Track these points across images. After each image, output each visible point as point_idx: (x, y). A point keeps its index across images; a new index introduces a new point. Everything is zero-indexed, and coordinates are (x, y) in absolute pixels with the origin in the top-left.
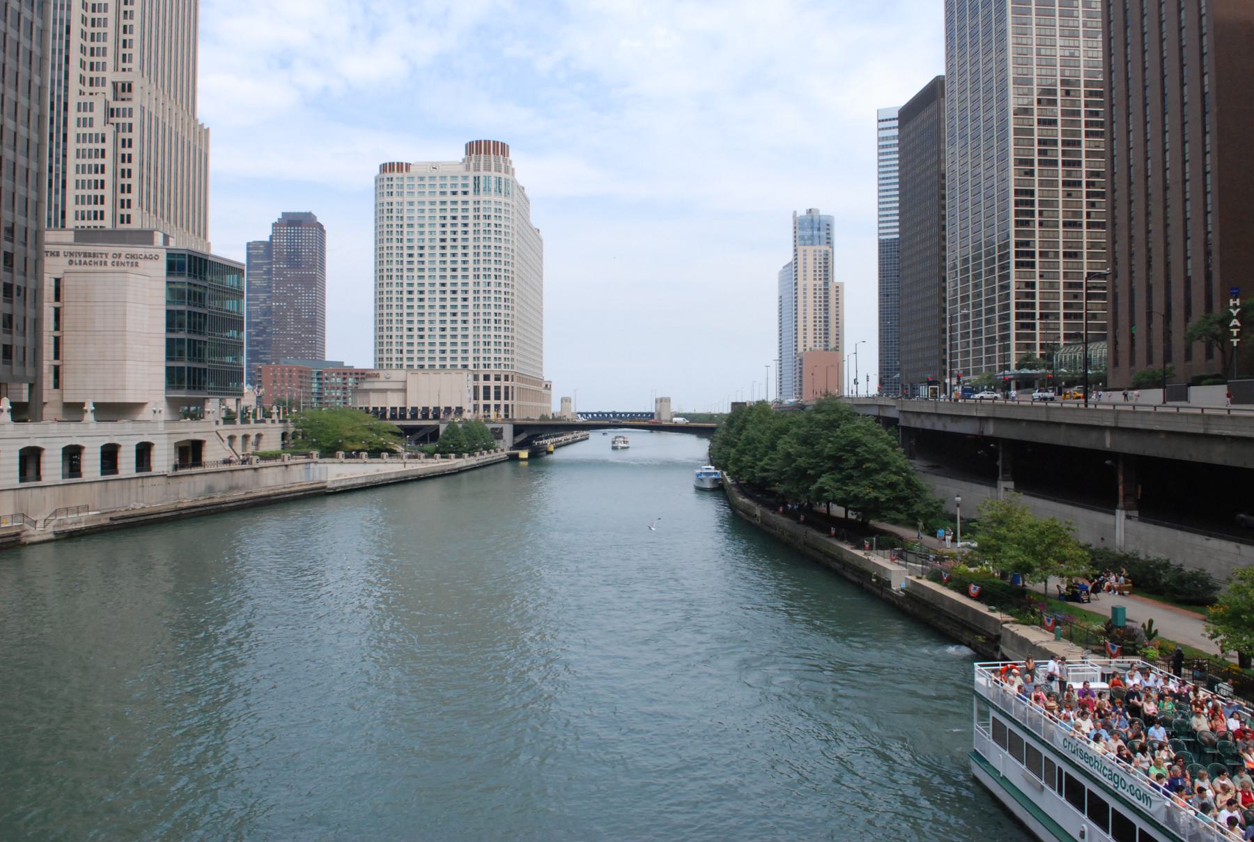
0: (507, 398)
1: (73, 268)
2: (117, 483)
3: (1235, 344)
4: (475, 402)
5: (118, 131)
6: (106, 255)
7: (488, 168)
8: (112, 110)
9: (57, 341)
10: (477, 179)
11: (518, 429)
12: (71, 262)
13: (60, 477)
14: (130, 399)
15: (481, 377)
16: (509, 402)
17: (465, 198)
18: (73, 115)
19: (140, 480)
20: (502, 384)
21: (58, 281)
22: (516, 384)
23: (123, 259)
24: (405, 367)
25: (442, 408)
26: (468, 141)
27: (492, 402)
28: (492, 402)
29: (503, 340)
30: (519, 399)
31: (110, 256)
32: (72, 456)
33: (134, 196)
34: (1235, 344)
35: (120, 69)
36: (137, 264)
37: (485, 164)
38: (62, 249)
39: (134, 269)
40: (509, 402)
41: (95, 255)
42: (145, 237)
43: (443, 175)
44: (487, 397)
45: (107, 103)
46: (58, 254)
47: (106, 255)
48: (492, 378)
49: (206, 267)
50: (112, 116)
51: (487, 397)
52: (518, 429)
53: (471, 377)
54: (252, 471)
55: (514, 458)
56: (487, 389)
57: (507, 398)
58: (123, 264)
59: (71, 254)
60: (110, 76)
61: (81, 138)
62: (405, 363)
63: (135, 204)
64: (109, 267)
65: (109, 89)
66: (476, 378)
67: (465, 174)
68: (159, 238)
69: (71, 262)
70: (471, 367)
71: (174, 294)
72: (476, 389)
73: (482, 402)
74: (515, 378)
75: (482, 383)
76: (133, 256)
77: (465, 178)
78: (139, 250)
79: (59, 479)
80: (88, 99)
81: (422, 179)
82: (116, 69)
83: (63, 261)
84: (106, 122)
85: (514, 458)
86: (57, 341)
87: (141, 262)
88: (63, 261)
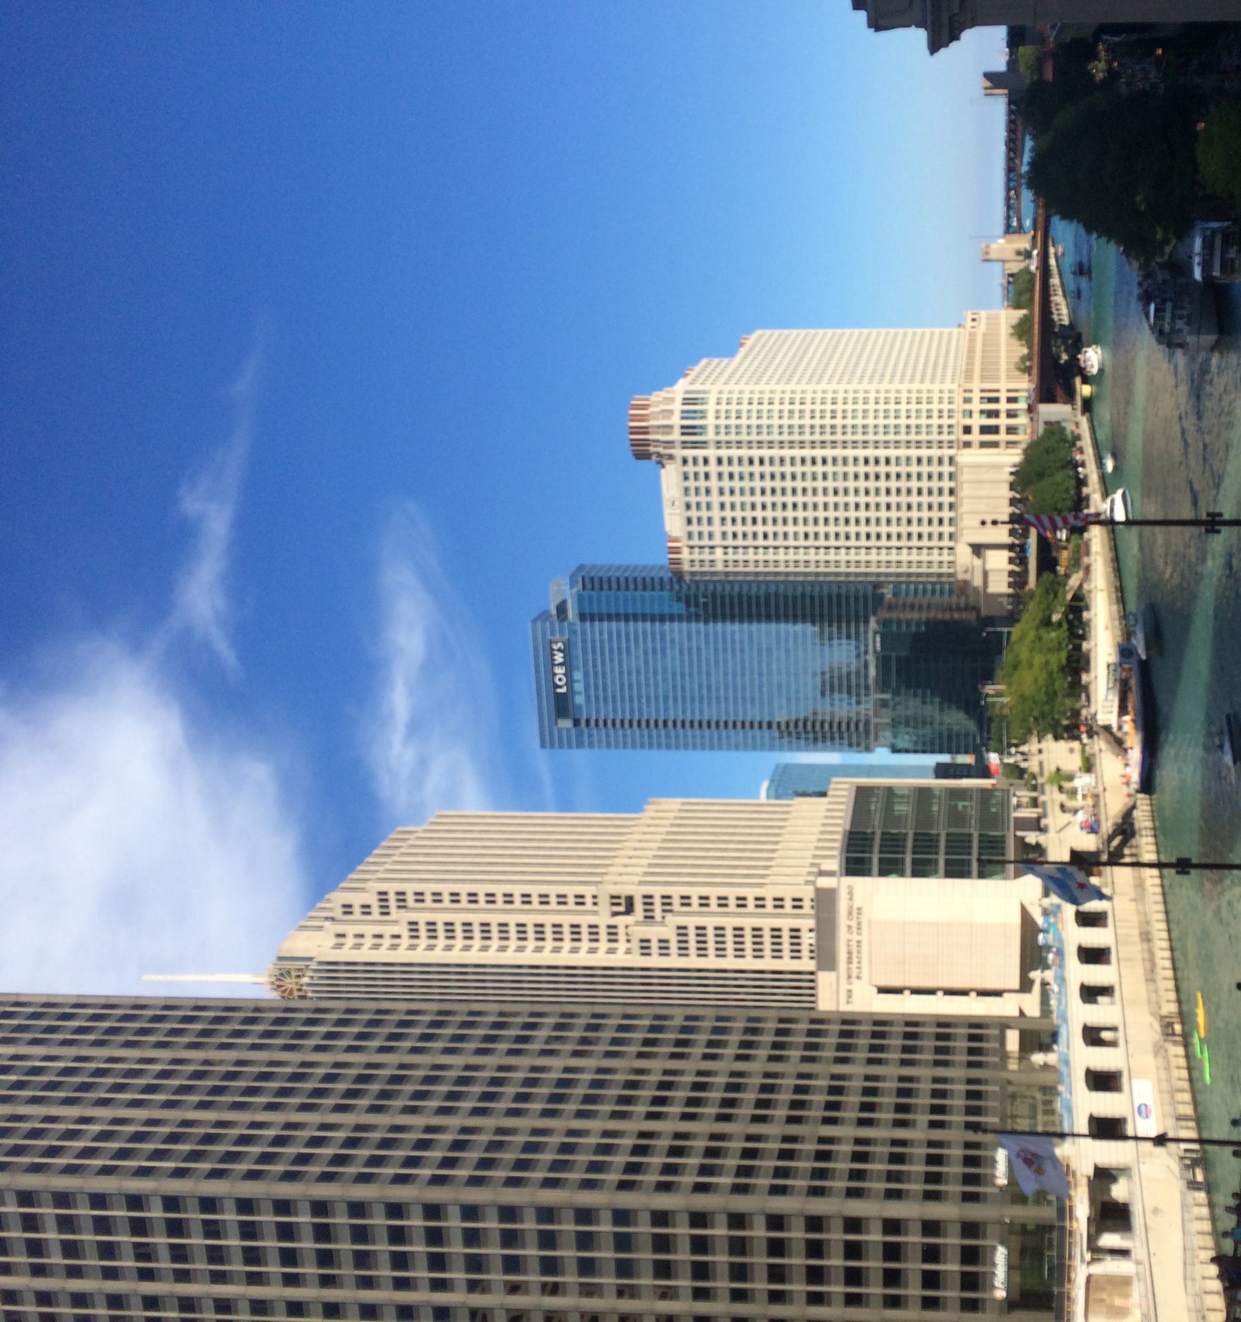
0: (996, 400)
1: (865, 974)
2: (1120, 948)
3: (1062, 362)
4: (1003, 445)
5: (670, 911)
6: (849, 941)
7: (668, 428)
8: (646, 917)
9: (950, 992)
10: (685, 445)
11: (1046, 394)
12: (859, 978)
13: (1114, 1008)
14: (1016, 919)
15: (967, 438)
16: (1003, 396)
17: (713, 461)
18: (655, 961)
19: (1117, 924)
20: (976, 406)
21: (883, 990)
22: (976, 385)
23: (854, 923)
24: (951, 544)
25: (1012, 494)
26: (633, 458)
27: (1003, 421)
28: (1003, 421)
29: (913, 407)
30: (996, 379)
31: (850, 937)
32: (1091, 993)
33: (750, 893)
34: (1062, 362)
35: (595, 908)
36: (859, 909)
37: (664, 433)
38: (844, 986)
39: (864, 911)
40: (1003, 396)
41: (850, 953)
42: (825, 902)
43: (682, 491)
44: (994, 430)
45: (637, 923)
46: (849, 991)
47: (849, 941)
48: (967, 422)
49: (859, 833)
50: (652, 917)
51: (994, 430)
52: (1046, 394)
53: (967, 451)
54: (1106, 793)
55: (1088, 405)
56: (985, 430)
57: (996, 400)
58: (859, 924)
59: (849, 977)
60: (603, 919)
61: (683, 950)
62: (946, 543)
63: (759, 892)
64: (864, 938)
65: (621, 921)
66: (967, 445)
67: (679, 461)
68: (824, 882)
69: (859, 978)
70: (952, 452)
71: (890, 868)
72: (983, 445)
73: (1002, 437)
74: (968, 386)
75: (975, 437)
76: (850, 913)
77: (685, 461)
78: (842, 906)
79: (1117, 1008)
80: (635, 945)
81: (689, 521)
82: (595, 913)
83: (857, 986)
84: (662, 923)
85: (1088, 405)
86: (950, 992)
87: (857, 904)
88: (857, 986)
